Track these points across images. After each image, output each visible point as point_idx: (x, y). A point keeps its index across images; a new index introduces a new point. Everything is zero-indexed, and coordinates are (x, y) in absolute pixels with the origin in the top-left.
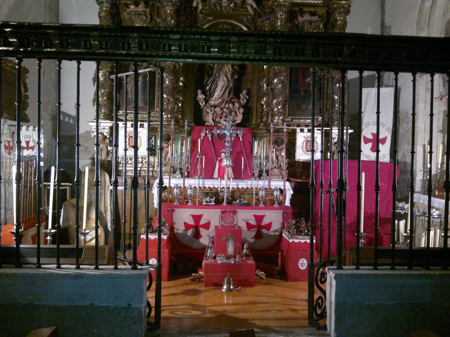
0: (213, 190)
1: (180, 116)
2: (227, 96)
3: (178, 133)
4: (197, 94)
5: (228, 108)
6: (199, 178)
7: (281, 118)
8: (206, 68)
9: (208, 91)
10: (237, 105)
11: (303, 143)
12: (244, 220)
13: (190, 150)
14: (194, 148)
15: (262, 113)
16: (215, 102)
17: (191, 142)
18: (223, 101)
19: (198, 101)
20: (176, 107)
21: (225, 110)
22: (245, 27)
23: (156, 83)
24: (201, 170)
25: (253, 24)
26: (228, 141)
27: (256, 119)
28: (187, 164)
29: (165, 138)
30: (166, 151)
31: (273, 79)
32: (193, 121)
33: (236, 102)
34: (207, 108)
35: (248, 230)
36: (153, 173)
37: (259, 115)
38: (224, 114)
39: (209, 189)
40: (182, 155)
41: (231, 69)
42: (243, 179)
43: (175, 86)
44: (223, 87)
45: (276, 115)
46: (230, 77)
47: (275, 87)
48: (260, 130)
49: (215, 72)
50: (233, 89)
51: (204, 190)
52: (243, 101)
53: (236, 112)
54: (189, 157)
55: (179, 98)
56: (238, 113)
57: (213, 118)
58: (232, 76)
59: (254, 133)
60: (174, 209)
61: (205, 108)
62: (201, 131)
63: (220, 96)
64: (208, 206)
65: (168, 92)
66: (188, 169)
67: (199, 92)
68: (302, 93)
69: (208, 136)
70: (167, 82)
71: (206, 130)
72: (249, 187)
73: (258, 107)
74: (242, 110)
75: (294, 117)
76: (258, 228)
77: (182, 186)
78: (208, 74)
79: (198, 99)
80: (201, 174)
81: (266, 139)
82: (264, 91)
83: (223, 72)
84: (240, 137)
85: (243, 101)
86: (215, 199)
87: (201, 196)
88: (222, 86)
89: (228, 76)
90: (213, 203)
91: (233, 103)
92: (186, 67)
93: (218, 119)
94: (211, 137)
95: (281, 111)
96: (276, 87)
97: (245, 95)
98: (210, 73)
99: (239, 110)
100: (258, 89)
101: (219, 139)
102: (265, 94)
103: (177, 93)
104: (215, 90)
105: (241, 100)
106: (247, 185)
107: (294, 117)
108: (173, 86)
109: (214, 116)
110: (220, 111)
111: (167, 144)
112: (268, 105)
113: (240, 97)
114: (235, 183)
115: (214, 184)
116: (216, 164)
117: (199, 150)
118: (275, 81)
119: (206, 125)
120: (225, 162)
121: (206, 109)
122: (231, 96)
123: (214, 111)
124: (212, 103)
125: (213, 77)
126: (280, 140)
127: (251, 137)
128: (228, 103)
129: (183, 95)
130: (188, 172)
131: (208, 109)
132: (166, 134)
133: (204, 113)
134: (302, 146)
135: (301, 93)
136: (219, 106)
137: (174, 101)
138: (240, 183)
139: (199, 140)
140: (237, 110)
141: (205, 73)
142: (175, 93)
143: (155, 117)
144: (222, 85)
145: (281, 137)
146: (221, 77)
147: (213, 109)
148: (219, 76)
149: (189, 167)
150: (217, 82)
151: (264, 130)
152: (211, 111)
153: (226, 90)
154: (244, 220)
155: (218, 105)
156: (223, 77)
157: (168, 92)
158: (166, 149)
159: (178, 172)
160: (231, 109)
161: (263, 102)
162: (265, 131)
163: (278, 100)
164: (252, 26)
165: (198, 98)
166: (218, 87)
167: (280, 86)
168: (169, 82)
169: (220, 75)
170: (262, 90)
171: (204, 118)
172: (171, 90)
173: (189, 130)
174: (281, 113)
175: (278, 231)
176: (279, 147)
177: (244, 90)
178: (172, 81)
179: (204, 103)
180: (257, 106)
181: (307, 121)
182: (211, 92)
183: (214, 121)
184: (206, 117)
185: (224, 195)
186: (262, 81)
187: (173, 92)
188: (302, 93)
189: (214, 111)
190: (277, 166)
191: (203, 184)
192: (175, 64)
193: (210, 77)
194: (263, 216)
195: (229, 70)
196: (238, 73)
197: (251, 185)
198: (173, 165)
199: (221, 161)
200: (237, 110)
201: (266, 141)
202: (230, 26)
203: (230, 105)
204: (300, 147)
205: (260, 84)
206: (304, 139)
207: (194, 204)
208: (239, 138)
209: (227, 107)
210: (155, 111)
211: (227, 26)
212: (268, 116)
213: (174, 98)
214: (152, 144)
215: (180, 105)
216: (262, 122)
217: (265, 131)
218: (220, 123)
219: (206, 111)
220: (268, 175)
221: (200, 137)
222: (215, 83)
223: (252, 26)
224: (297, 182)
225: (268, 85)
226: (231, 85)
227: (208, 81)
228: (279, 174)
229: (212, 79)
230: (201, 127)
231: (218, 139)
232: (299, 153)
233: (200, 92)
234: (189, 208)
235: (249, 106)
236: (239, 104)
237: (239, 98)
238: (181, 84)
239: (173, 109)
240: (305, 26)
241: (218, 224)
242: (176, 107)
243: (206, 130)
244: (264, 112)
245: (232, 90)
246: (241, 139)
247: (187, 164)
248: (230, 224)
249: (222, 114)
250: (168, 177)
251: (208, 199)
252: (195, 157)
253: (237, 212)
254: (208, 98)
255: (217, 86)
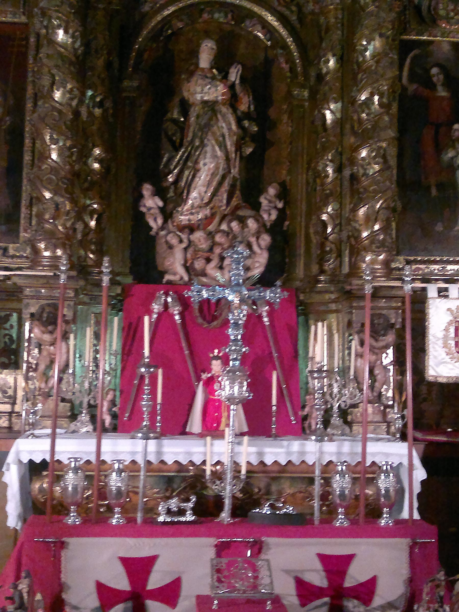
0: (188, 471)
1: (91, 256)
2: (225, 202)
3: (84, 304)
4: (141, 196)
5: (227, 234)
6: (147, 438)
7: (381, 257)
8: (165, 126)
9: (172, 187)
10: (252, 224)
11: (447, 330)
12: (287, 572)
13: (120, 351)
14: (132, 345)
15: (322, 245)
16: (191, 217)
17: (123, 329)
18: (213, 215)
19: (143, 214)
20: (79, 226)
21: (218, 238)
22: (272, 14)
23: (25, 162)
24: (153, 414)
25: (294, 8)
26: (236, 324)
27: (307, 266)
28: (111, 393)
29: (45, 315)
30: (50, 354)
31: (356, 149)
32: (127, 271)
33: (250, 217)
34: (169, 232)
35: (303, 605)
36: (10, 420)
37: (315, 252)
38: (217, 250)
39: (175, 467)
40: (97, 366)
41: (234, 127)
42: (277, 436)
43: (77, 167)
44: (213, 175)
45: (366, 250)
46: (233, 149)
47: (361, 171)
48: (320, 292)
49: (190, 135)
50: (241, 183)
51: (160, 471)
52: (270, 214)
53: (249, 246)
54: (119, 372)
55: (90, 205)
56: (255, 248)
57: (186, 261)
58: (239, 147)
59: (301, 303)
60: (64, 539)
61: (163, 233)
62: (151, 298)
63: (206, 200)
64: (171, 529)
65: (57, 184)
66: (115, 406)
67: (147, 190)
68: (434, 192)
69: (171, 310)
70: (54, 156)
71: (167, 294)
72: (296, 460)
73: (311, 231)
74: (266, 239)
75: (412, 258)
76: (332, 598)
77: (93, 459)
78: (173, 143)
79: (143, 209)
80: (152, 427)
81: (338, 318)
82: (329, 186)
83: (214, 134)
84: (265, 314)
85: (270, 214)
86: (196, 503)
87: (152, 488)
88: (211, 171)
89: (225, 146)
90: (189, 517)
91: (242, 221)
92: (111, 120)
93: (199, 265)
94: (181, 314)
95: (382, 237)
96: (365, 169)
97: (274, 199)
98: (178, 141)
99: (258, 238)
100: (311, 180)
101: (204, 319)
102: (331, 194)
103: (85, 191)
104: (190, 185)
105: (262, 213)
106: (289, 453)
107: (412, 258)
108: (72, 166)
109: (189, 256)
110: (206, 240)
111: (51, 332)
112: (340, 224)
113: (260, 204)
114: (253, 449)
115: (189, 453)
116: (194, 394)
117: (147, 351)
118: (364, 153)
119: (165, 280)
120: (227, 388)
121: (167, 235)
122: (234, 202)
123: (190, 241)
124: (183, 219)
125: (187, 148)
126: (381, 321)
127: (294, 316)
128: (228, 218)
129: (101, 198)
130: (114, 416)
131: (171, 235)
132: (49, 305)
133: (161, 248)
134: (446, 338)
135: (430, 193)
136: (201, 227)
137: (73, 209)
138: (267, 450)
139: (146, 319)
140: (253, 240)
141: (164, 140)
142: (77, 191)
143: (21, 257)
144: (209, 169)
145: (384, 312)
146: (208, 149)
147: (184, 236)
148: (203, 145)
149: (118, 401)
150: (196, 162)
151: (332, 293)
152: (181, 241)
153: (220, 184)
154: (287, 572)
155: (199, 225)
156: (213, 146)
157: (57, 184)
158: (48, 350)
159: (84, 417)
160: (235, 237)
161: (324, 217)
162: (333, 296)
163: (373, 207)
164: (292, 12)
165: (145, 206)
166: (198, 175)
167: (377, 167)
168: (59, 155)
169: (206, 141)
170: (323, 184)
171: (159, 261)
172: (65, 178)
173: (118, 295)
174: (382, 244)
175: (397, 604)
176: (377, 340)
177: (270, 184)
178: (67, 153)
179: (160, 221)
180: (307, 227)
181: (449, 267)
182: (180, 191)
183: (188, 268)
184: (165, 258)
185: (224, 489)
186: (322, 159)
187: (73, 184)
188: (434, 192)
189: (190, 241)
190: (370, 395)
191: (159, 453)
192: (77, 105)
193: (177, 150)
194: (349, 558)
195: (230, 129)
196: (254, 138)
197: (302, 453)
198: (69, 396)
199: (210, 382)
200: (253, 240)
201: (338, 324)
202: (230, 16)
203: (235, 225)
204: (439, 339)
205: (315, 168)
206: (451, 318)
207: (131, 521)
208: (260, 317)
209: (223, 231)
210: (21, 239)
211: (222, 14)
212: (340, 255)
213: (74, 201)
214: (11, 336)
215: (93, 223)
216: (322, 272)
217: (333, 296)
218: (204, 274)
219: (167, 242)
220: (346, 422)
221: (150, 312)
222: (190, 164)
223: (292, 12)
224: (430, 444)
225: (339, 170)
226: (235, 171)
227: (170, 159)
228: (378, 418)
229: (184, 153)
230: (151, 287)
231: (200, 320)
232: (435, 357)
233: (148, 189)
234: (115, 535)
235: (285, 228)
236: (257, 220)
237: (256, 207)
238: (96, 166)
239: (71, 232)
240: (441, 6)
241: (206, 591)
242: (79, 226)
243: (167, 294)
244: (328, 244)
245: (238, 183)
246: (266, 319)
247: (111, 393)
248: (250, 595)
249: (211, 250)
250: (49, 431)
251: (174, 503)
252: (133, 374)
253: (268, 544)
254: (171, 206)
255: (196, 171)
